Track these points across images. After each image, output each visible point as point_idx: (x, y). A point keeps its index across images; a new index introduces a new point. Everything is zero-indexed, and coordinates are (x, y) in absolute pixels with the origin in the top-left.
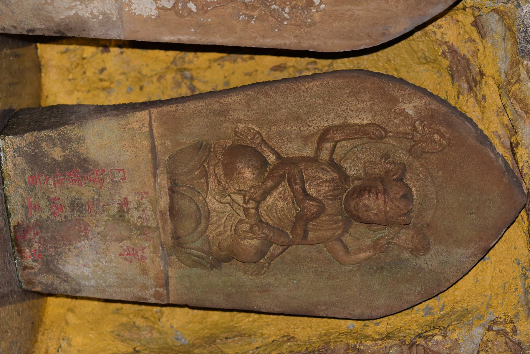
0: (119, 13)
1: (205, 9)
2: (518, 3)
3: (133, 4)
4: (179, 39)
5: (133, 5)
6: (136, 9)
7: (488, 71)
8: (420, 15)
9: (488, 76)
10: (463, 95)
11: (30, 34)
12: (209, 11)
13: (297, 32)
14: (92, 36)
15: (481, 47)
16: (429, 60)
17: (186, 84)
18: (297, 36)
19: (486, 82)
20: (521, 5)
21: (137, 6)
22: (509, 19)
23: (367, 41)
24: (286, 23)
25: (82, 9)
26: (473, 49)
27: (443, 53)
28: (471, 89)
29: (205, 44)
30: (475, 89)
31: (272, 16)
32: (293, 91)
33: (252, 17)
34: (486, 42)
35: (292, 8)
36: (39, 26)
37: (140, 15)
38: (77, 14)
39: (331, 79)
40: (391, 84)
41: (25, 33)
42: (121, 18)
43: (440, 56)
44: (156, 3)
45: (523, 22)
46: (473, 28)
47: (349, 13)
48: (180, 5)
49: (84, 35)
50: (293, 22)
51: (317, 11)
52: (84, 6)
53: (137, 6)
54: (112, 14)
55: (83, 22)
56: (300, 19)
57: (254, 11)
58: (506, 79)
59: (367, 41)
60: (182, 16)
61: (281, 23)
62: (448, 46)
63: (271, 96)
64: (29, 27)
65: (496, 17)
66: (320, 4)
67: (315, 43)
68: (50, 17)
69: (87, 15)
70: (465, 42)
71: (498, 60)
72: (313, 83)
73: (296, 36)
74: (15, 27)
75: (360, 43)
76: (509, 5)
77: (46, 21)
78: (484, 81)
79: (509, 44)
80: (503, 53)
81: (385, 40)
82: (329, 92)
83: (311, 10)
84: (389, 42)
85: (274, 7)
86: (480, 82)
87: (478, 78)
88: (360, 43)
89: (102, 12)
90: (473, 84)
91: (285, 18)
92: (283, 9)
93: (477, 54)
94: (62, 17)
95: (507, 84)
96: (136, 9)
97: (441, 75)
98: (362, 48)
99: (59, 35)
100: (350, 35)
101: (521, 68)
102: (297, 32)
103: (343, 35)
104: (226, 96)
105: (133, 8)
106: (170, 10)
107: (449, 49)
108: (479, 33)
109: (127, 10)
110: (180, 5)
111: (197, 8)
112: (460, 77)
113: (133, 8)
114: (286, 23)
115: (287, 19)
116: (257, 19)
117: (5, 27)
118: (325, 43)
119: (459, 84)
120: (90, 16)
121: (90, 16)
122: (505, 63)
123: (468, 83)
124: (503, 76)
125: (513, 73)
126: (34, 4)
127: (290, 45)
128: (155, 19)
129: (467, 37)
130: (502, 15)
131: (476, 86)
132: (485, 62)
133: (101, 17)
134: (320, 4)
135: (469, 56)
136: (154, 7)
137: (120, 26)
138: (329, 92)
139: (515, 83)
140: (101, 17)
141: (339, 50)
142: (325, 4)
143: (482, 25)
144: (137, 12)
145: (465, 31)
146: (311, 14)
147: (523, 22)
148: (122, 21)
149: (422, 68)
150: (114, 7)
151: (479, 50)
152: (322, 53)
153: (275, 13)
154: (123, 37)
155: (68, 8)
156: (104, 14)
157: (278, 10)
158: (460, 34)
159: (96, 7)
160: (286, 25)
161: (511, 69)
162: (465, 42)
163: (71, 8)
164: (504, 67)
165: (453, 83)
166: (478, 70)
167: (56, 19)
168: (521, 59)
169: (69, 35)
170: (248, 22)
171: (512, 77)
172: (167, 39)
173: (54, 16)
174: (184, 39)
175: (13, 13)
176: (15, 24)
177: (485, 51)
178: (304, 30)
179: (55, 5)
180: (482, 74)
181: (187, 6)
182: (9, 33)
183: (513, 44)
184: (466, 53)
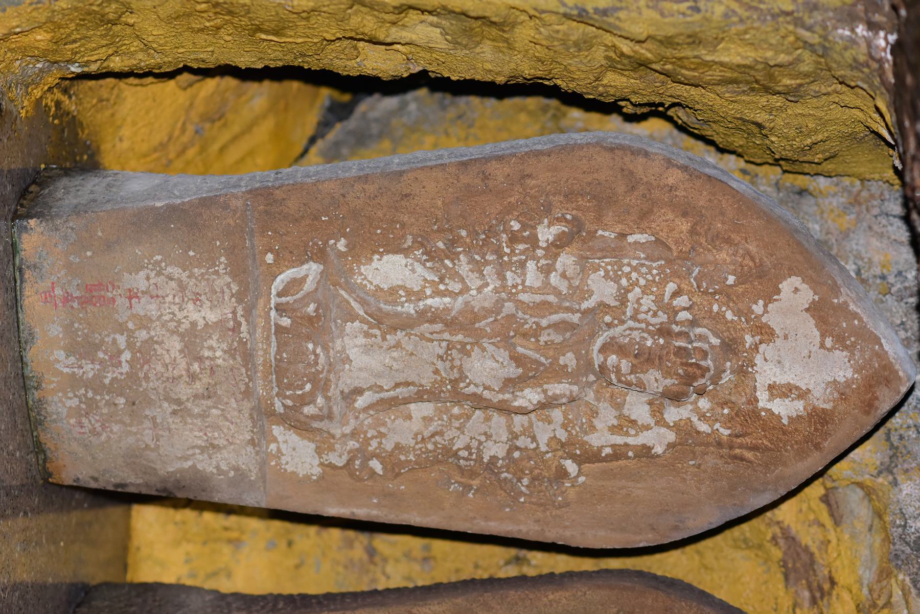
0: (260, 469)
1: (397, 470)
2: (895, 478)
3: (283, 455)
4: (353, 513)
5: (283, 458)
6: (287, 463)
7: (843, 578)
8: (735, 505)
9: (843, 587)
10: (801, 609)
11: (119, 490)
12: (402, 474)
13: (539, 515)
14: (216, 500)
15: (832, 536)
16: (751, 544)
17: (362, 543)
18: (539, 521)
19: (838, 595)
20: (899, 482)
21: (289, 459)
22: (879, 501)
23: (650, 536)
24: (522, 500)
25: (203, 461)
26: (821, 538)
27: (774, 538)
28: (814, 601)
29: (394, 522)
30: (820, 603)
31: (501, 488)
32: (528, 603)
33: (470, 487)
34: (842, 531)
35: (533, 479)
36: (134, 481)
37: (293, 473)
38: (194, 466)
39: (589, 589)
40: (683, 604)
41: (111, 488)
42: (263, 477)
43: (768, 541)
44: (320, 457)
45: (901, 509)
46: (823, 506)
47: (624, 492)
48: (357, 462)
49: (204, 497)
50: (534, 500)
51: (573, 486)
52: (206, 456)
53: (289, 459)
54: (250, 470)
55: (203, 480)
56: (545, 495)
57: (473, 479)
58: (870, 597)
59: (650, 536)
60: (360, 479)
61: (515, 499)
62: (781, 528)
63: (493, 608)
64: (118, 481)
65: (860, 493)
66: (578, 476)
67: (568, 533)
68: (151, 468)
69: (211, 469)
70: (809, 526)
71: (858, 563)
72: (560, 593)
73: (537, 521)
74: (95, 479)
75: (638, 538)
76: (880, 480)
77: (145, 473)
78: (834, 592)
79: (878, 539)
80: (867, 552)
81: (678, 536)
82: (585, 608)
83: (563, 483)
84: (683, 540)
85: (504, 475)
86: (830, 594)
87: (826, 586)
88: (638, 538)
89: (234, 466)
90: (818, 595)
91: (522, 492)
92: (519, 480)
93: (827, 547)
94: (171, 470)
95: (870, 606)
96: (287, 463)
97: (769, 569)
98: (641, 545)
99: (164, 495)
100: (624, 524)
101: (894, 585)
102: (539, 515)
103: (612, 524)
104: (421, 603)
105: (284, 462)
106: (341, 468)
107: (783, 534)
108: (832, 515)
109: (273, 463)
110: (357, 462)
111: (384, 469)
112: (798, 580)
113: (284, 462)
114: (522, 500)
115: (525, 495)
116: (477, 490)
117: (80, 477)
118: (583, 534)
119: (796, 591)
120: (215, 471)
121: (215, 471)
122: (870, 569)
123: (811, 591)
124: (865, 591)
125: (881, 589)
126: (128, 448)
127: (527, 533)
128: (317, 481)
129: (812, 517)
130: (869, 492)
131: (822, 598)
132: (838, 563)
133: (232, 474)
134: (578, 476)
135: (814, 549)
136: (316, 462)
137: (262, 489)
138: (585, 608)
139: (883, 608)
140: (232, 474)
141: (604, 547)
142: (586, 476)
143: (837, 503)
144: (290, 468)
145: (810, 508)
146: (564, 489)
147: (901, 509)
148: (264, 482)
149: (739, 554)
150: (254, 461)
151: (829, 542)
152: (578, 548)
153: (506, 484)
154: (265, 503)
155: (181, 458)
156: (236, 469)
157: (510, 481)
158: (801, 511)
159: (226, 460)
160: (523, 503)
161: (879, 581)
162: (809, 526)
163: (186, 459)
164: (868, 576)
165: (786, 587)
166: (826, 572)
167: (162, 473)
168: (895, 572)
169: (180, 495)
170: (463, 494)
171: (880, 596)
172: (332, 511)
173: (158, 467)
174: (361, 513)
175: (93, 458)
176: (96, 475)
177: (838, 545)
178: (551, 513)
179: (161, 452)
180: (833, 583)
181: (368, 465)
182: (86, 486)
183: (883, 540)
184: (810, 543)
